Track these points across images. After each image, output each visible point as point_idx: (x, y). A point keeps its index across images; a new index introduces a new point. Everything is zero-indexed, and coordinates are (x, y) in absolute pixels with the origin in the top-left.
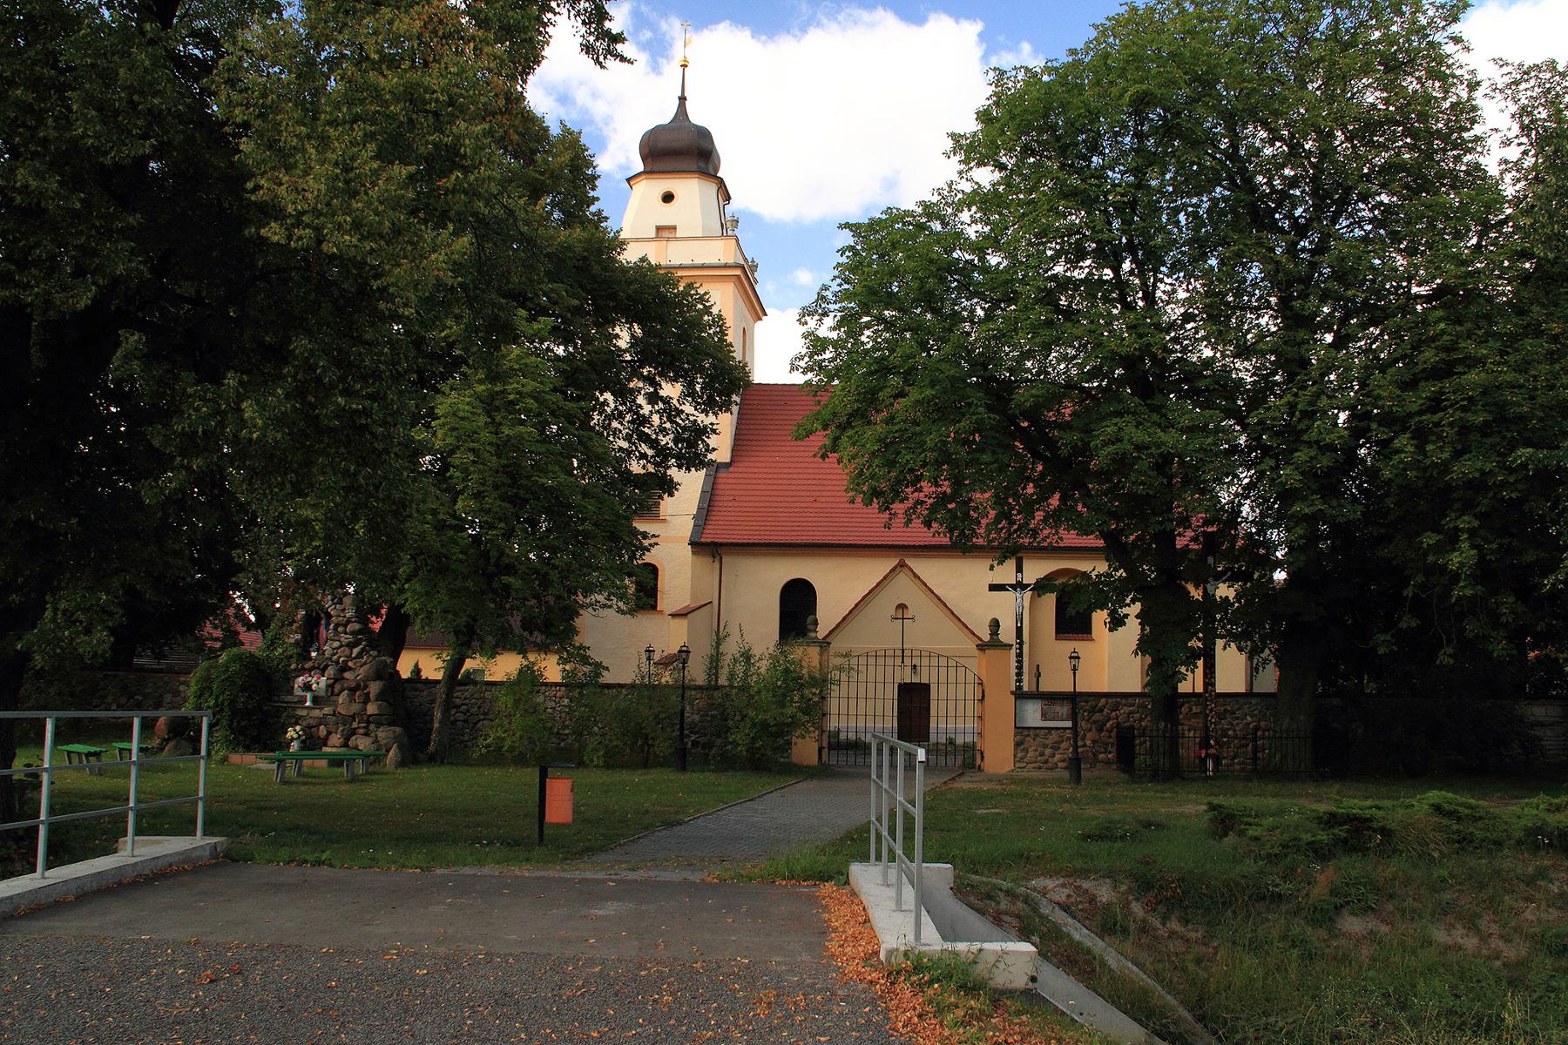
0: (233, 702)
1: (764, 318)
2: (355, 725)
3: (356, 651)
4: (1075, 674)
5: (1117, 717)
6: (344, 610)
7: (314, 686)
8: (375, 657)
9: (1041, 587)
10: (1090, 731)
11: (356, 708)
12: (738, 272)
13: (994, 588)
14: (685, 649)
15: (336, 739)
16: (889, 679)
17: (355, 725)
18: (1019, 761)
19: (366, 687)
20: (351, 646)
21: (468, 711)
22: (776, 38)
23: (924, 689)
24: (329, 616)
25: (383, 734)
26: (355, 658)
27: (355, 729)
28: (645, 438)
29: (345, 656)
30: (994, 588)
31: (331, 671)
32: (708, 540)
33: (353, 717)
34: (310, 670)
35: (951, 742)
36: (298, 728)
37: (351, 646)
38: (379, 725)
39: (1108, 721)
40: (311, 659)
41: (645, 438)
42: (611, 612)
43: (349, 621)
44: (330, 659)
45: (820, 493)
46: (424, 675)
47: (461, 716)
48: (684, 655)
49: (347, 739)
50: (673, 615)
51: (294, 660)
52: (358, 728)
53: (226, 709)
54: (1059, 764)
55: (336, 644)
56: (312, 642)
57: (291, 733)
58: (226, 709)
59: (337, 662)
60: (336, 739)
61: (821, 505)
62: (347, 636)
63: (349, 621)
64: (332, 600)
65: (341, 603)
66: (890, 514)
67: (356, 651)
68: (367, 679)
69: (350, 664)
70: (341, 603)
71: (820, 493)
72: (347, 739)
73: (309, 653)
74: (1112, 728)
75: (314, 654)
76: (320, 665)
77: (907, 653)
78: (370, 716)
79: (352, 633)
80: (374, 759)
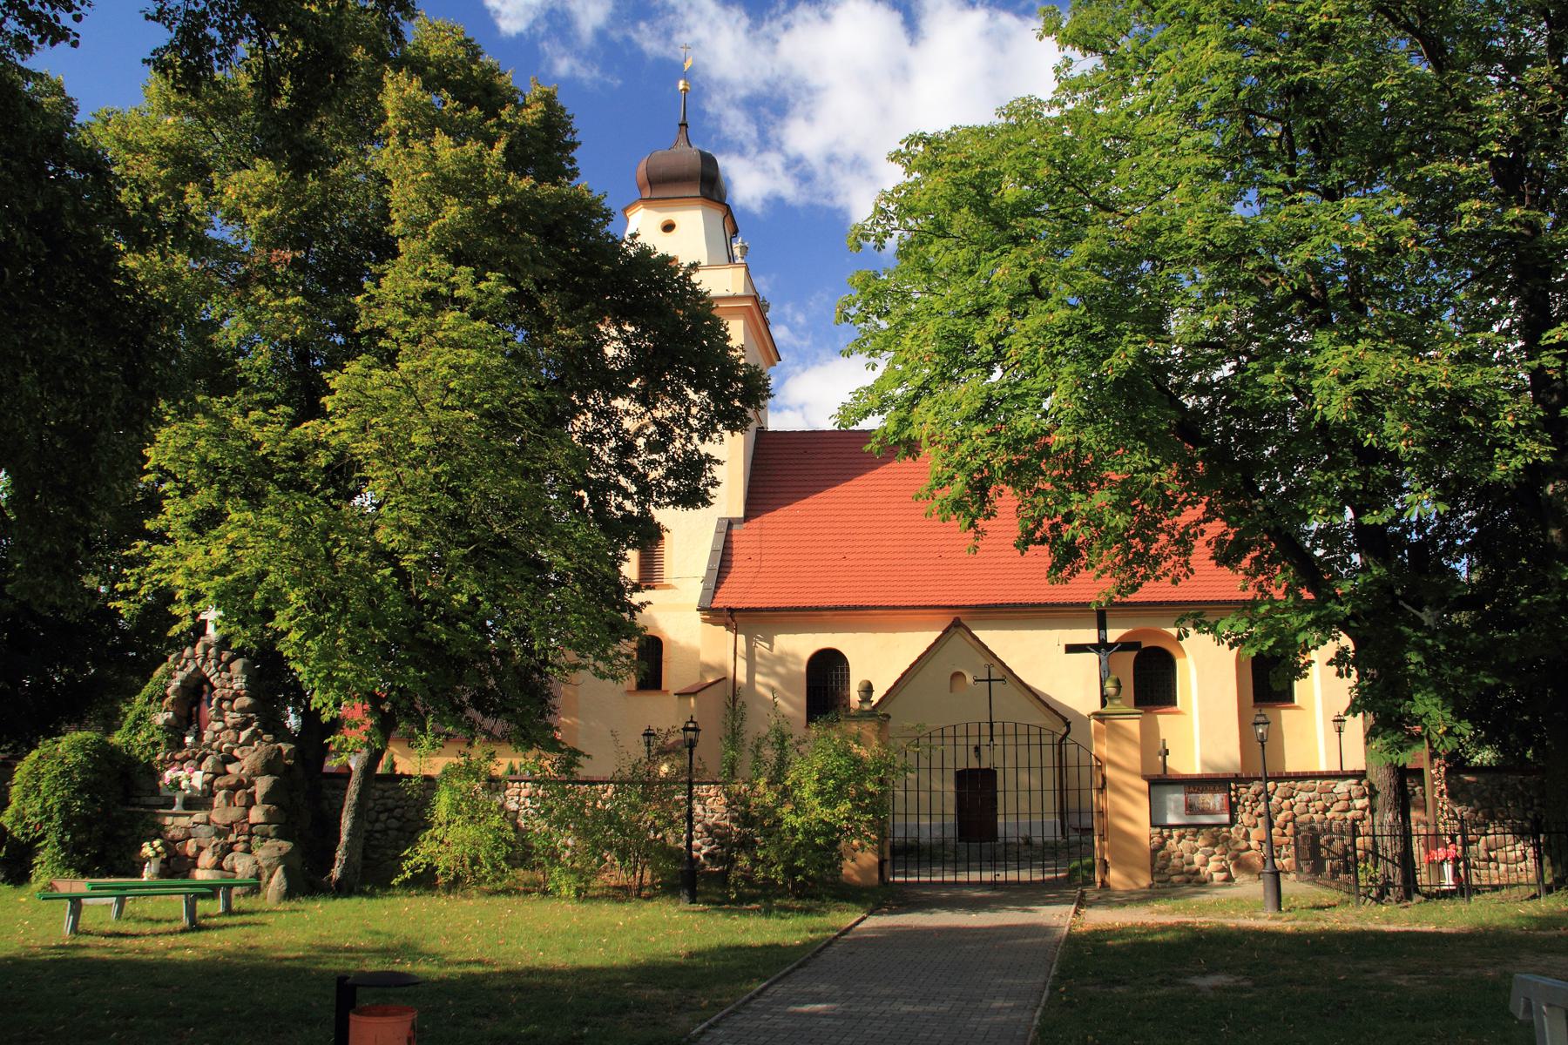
0: (65, 807)
1: (778, 363)
2: (232, 838)
3: (244, 735)
5: (1292, 807)
6: (230, 679)
8: (269, 743)
9: (1124, 645)
11: (234, 813)
12: (749, 304)
13: (1071, 649)
14: (691, 725)
15: (206, 859)
17: (232, 838)
18: (1159, 873)
19: (252, 783)
21: (403, 816)
24: (213, 688)
29: (230, 742)
30: (1071, 649)
31: (208, 763)
32: (721, 605)
33: (231, 826)
34: (183, 761)
35: (1028, 842)
36: (157, 843)
42: (585, 675)
43: (237, 695)
44: (209, 746)
45: (850, 550)
48: (691, 734)
49: (222, 858)
50: (680, 694)
51: (163, 747)
53: (56, 817)
54: (1216, 876)
55: (219, 725)
56: (190, 724)
57: (147, 850)
58: (56, 817)
61: (852, 563)
62: (235, 715)
63: (237, 695)
64: (216, 666)
66: (977, 532)
67: (244, 735)
69: (236, 753)
71: (850, 550)
73: (183, 737)
76: (195, 754)
77: (997, 728)
78: (253, 825)
79: (241, 710)
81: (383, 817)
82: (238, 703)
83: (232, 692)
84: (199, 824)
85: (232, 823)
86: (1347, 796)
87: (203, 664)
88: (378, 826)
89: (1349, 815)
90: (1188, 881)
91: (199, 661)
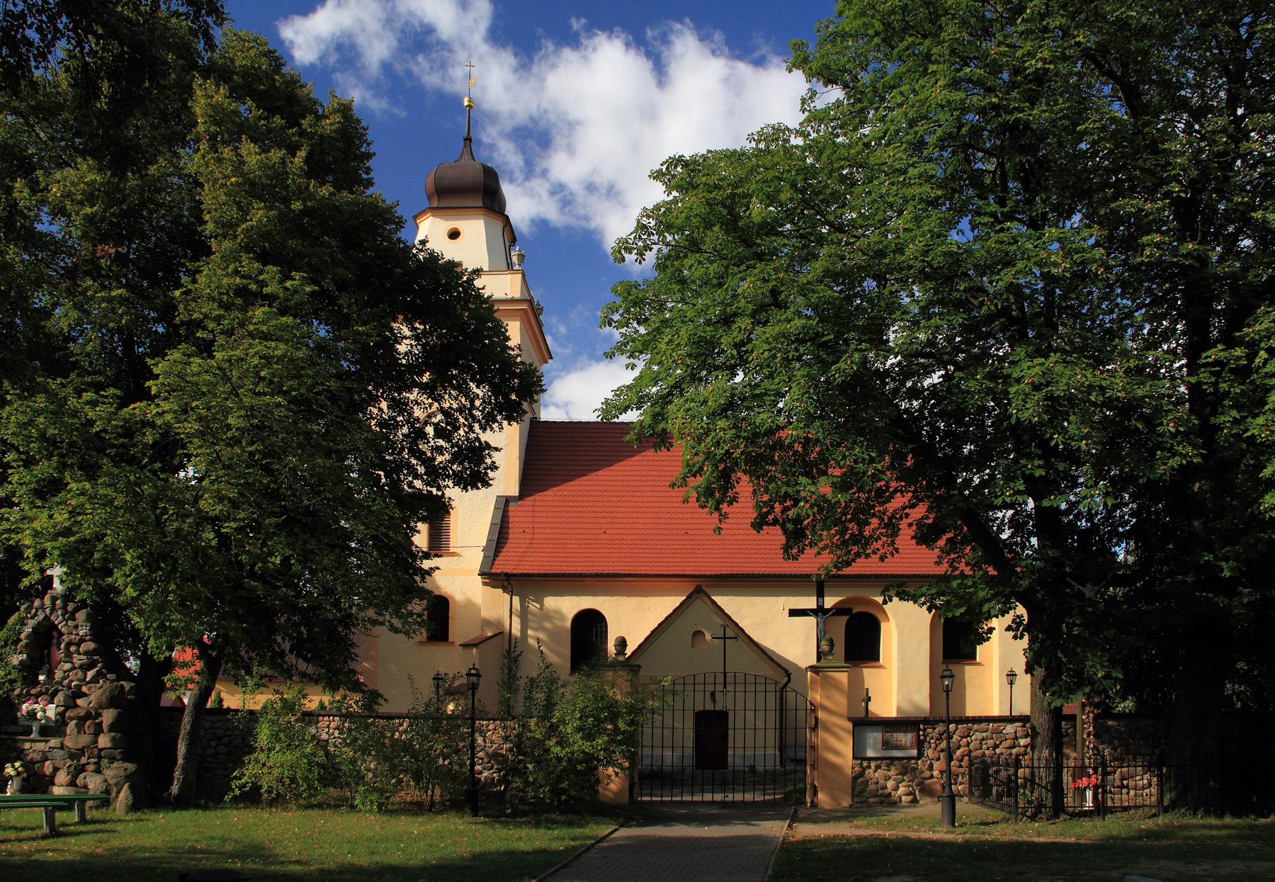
3: (90, 674)
4: (948, 695)
5: (968, 744)
6: (76, 627)
7: (39, 715)
8: (113, 681)
9: (838, 610)
10: (938, 759)
11: (84, 740)
13: (794, 613)
14: (473, 672)
15: (62, 777)
16: (689, 706)
17: (84, 760)
18: (857, 796)
19: (100, 715)
20: (85, 668)
22: (632, 52)
23: (722, 716)
24: (61, 634)
25: (114, 771)
26: (89, 683)
27: (84, 765)
28: (419, 455)
29: (78, 680)
30: (794, 613)
31: (60, 697)
34: (37, 696)
35: (753, 769)
37: (85, 668)
38: (112, 759)
39: (958, 748)
40: (38, 683)
41: (419, 455)
43: (82, 640)
44: (60, 683)
46: (226, 705)
47: (222, 749)
49: (75, 777)
51: (19, 684)
52: (89, 764)
59: (70, 688)
60: (62, 777)
63: (82, 640)
64: (63, 615)
65: (74, 619)
67: (90, 674)
68: (101, 706)
69: (84, 689)
70: (74, 619)
72: (75, 777)
74: (963, 756)
75: (42, 678)
77: (730, 678)
78: (101, 750)
79: (86, 653)
80: (105, 801)
81: (213, 744)
82: (83, 648)
83: (78, 638)
84: (54, 748)
85: (83, 748)
86: (1013, 736)
87: (51, 613)
88: (209, 751)
89: (1014, 751)
90: (882, 802)
91: (48, 611)
